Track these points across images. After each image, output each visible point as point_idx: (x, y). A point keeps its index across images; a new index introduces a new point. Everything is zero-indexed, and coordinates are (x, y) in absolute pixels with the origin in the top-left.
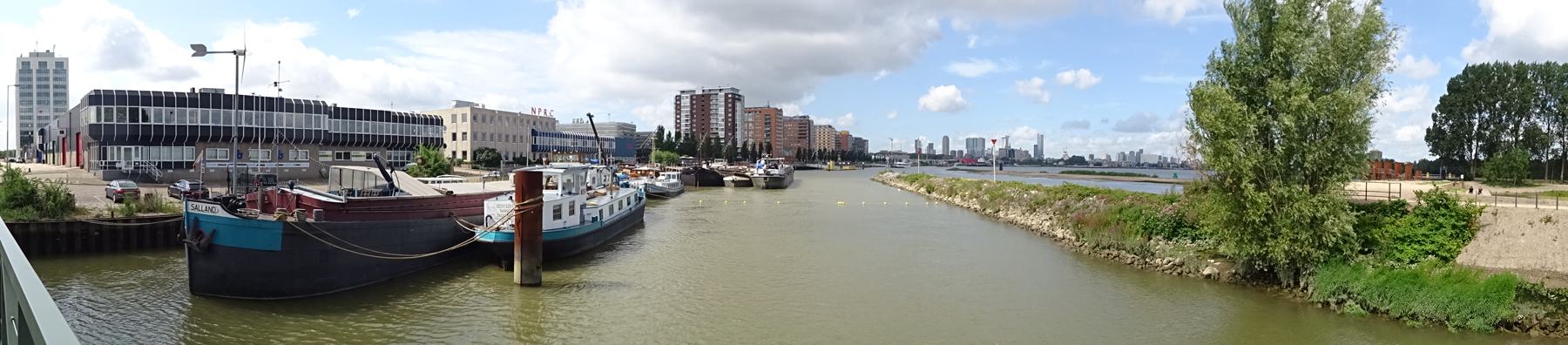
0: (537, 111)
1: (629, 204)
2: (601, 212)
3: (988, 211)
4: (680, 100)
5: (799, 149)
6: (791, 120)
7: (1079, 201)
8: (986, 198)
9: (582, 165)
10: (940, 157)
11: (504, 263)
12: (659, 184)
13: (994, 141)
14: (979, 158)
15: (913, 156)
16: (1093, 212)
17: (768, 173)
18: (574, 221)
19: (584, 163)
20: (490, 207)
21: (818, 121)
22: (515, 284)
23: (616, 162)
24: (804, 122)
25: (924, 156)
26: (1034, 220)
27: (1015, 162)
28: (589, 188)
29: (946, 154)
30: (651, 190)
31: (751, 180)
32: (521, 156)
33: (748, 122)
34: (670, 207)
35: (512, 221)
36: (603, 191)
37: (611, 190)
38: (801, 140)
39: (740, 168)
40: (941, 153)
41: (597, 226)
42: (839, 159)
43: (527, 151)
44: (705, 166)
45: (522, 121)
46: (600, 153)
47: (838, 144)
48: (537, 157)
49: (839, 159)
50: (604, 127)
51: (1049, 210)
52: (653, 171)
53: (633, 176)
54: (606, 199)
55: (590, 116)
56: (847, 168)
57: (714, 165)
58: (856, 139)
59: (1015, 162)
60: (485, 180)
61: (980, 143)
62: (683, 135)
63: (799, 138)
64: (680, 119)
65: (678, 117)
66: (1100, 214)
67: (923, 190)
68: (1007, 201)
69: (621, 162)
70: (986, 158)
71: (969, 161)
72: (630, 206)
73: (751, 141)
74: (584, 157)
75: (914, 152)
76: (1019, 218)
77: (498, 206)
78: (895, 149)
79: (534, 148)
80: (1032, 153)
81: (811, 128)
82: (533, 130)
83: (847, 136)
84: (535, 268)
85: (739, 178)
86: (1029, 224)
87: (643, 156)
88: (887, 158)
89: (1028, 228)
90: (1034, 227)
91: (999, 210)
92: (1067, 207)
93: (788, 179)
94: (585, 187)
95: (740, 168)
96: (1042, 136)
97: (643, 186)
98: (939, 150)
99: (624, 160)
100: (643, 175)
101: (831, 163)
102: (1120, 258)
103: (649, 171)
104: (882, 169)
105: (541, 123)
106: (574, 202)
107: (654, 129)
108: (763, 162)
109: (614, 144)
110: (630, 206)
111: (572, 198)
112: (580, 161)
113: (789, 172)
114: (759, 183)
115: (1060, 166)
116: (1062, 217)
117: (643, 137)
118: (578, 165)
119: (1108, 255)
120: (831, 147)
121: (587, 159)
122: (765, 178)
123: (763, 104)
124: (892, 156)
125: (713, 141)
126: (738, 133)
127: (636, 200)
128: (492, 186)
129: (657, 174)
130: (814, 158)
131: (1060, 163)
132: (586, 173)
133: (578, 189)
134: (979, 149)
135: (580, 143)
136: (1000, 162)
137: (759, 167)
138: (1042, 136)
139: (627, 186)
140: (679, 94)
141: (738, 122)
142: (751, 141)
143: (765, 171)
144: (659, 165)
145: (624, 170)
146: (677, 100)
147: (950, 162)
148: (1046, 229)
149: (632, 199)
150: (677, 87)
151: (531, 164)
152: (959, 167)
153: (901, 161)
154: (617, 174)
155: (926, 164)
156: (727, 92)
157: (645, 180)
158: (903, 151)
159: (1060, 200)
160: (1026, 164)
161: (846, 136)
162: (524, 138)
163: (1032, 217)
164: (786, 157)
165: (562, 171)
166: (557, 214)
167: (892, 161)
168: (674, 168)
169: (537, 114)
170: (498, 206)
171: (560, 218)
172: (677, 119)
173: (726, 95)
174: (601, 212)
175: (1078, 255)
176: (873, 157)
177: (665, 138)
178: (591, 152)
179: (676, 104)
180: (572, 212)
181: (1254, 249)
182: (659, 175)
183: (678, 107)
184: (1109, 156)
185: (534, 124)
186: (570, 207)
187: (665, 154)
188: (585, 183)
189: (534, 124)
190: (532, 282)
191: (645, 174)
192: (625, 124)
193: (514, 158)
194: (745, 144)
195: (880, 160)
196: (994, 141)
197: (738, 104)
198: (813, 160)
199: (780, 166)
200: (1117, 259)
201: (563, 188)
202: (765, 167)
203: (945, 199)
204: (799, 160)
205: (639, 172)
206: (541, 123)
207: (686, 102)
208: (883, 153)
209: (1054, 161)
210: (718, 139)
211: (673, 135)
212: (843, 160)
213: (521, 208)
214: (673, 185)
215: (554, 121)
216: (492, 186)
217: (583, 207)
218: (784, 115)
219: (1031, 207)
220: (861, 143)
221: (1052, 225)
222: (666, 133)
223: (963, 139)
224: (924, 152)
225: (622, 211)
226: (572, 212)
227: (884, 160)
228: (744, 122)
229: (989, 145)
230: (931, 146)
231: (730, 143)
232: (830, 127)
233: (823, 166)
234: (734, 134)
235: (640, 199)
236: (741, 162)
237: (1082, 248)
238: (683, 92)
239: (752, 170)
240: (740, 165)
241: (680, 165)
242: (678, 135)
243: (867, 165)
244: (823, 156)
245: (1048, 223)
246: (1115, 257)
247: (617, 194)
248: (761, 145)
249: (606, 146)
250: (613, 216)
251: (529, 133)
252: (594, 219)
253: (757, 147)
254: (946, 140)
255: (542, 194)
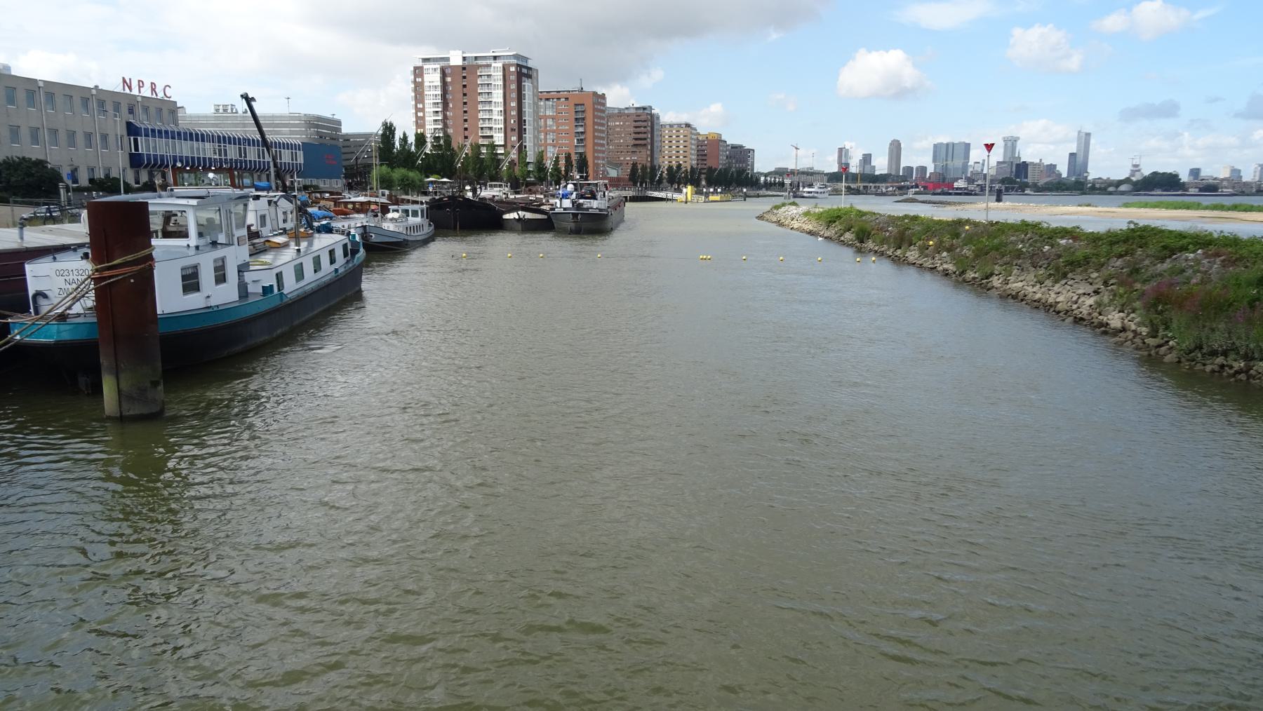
0: (135, 85)
1: (332, 261)
2: (279, 277)
3: (970, 275)
4: (421, 75)
5: (634, 165)
6: (621, 114)
7: (1163, 260)
8: (967, 251)
9: (238, 192)
10: (883, 178)
11: (82, 380)
12: (388, 226)
13: (989, 147)
14: (956, 180)
15: (834, 178)
16: (1194, 281)
17: (579, 206)
18: (226, 295)
19: (242, 187)
20: (38, 276)
21: (667, 116)
22: (109, 418)
23: (305, 188)
24: (643, 118)
25: (854, 177)
26: (1061, 294)
27: (1026, 186)
28: (253, 235)
29: (893, 173)
30: (374, 238)
31: (549, 217)
32: (107, 176)
33: (546, 117)
34: (407, 270)
35: (90, 301)
36: (281, 240)
37: (297, 238)
38: (640, 149)
39: (532, 197)
40: (885, 172)
41: (275, 303)
42: (704, 183)
43: (118, 164)
44: (469, 195)
45: (102, 103)
46: (272, 169)
47: (701, 155)
48: (144, 177)
49: (704, 183)
50: (280, 122)
51: (1095, 275)
52: (376, 203)
53: (338, 213)
54: (288, 255)
55: (248, 100)
56: (717, 198)
57: (486, 193)
58: (734, 147)
59: (1026, 186)
60: (23, 223)
61: (959, 152)
62: (429, 140)
63: (635, 145)
64: (423, 110)
65: (420, 106)
66: (1209, 287)
67: (848, 236)
68: (1007, 259)
69: (316, 187)
70: (970, 180)
71: (937, 185)
72: (336, 266)
73: (551, 153)
74: (241, 177)
75: (836, 170)
76: (1030, 289)
77: (60, 273)
78: (803, 164)
79: (136, 161)
80: (1063, 170)
81: (656, 127)
82: (129, 125)
83: (717, 142)
84: (148, 385)
85: (529, 215)
86: (1051, 300)
87: (357, 177)
88: (787, 181)
89: (1049, 308)
90: (1060, 307)
91: (992, 274)
92: (1135, 271)
93: (615, 215)
94: (244, 232)
95: (532, 197)
96: (1088, 135)
97: (361, 231)
98: (881, 165)
99: (322, 185)
100: (358, 211)
101: (688, 190)
102: (1249, 377)
103: (369, 203)
104: (779, 201)
105: (146, 109)
106: (223, 259)
107: (375, 128)
108: (570, 187)
109: (300, 154)
110: (336, 266)
111: (219, 253)
112: (233, 185)
113: (618, 205)
114: (565, 224)
115: (1123, 193)
116: (1121, 291)
117: (353, 143)
118: (230, 191)
119: (1222, 366)
120: (689, 161)
121: (247, 181)
122: (575, 215)
123: (572, 86)
124: (796, 179)
125: (484, 150)
126: (528, 136)
127: (345, 255)
128: (36, 237)
129: (385, 209)
130: (660, 181)
131: (1123, 188)
132: (246, 205)
133: (230, 235)
134: (958, 163)
135: (232, 153)
136: (997, 186)
137: (565, 196)
138: (1088, 135)
139: (328, 230)
140: (420, 64)
141: (528, 117)
142: (551, 153)
143: (573, 203)
144: (387, 192)
145: (322, 203)
146: (416, 75)
147: (900, 188)
148: (1085, 311)
149: (339, 253)
150: (415, 55)
151: (128, 189)
152: (917, 197)
153: (811, 186)
154: (310, 210)
155: (857, 192)
156: (507, 61)
157: (360, 220)
158: (817, 168)
159: (1120, 256)
160: (1050, 189)
161: (716, 142)
162: (111, 139)
163: (1057, 287)
164: (611, 180)
165: (194, 202)
166: (191, 282)
167: (795, 187)
168: (415, 198)
169: (135, 92)
170: (60, 273)
171: (198, 290)
172: (417, 110)
173: (505, 68)
174: (279, 277)
175: (1151, 361)
176: (762, 179)
177: (397, 144)
178: (256, 169)
179: (415, 82)
180: (221, 278)
181: (397, 183)
182: (388, 211)
183: (419, 89)
184: (1236, 172)
185: (131, 111)
186: (216, 269)
187: (398, 173)
188: (242, 222)
189: (131, 111)
190: (145, 410)
191: (362, 208)
192: (319, 118)
193: (91, 181)
194: (540, 158)
195: (775, 184)
196: (989, 147)
197: (527, 84)
198: (658, 185)
199: (599, 195)
200: (1243, 377)
201: (200, 235)
202: (574, 196)
203: (890, 253)
204: (635, 185)
205: (350, 206)
206: (146, 109)
207: (432, 78)
208: (781, 172)
209: (1110, 183)
210: (493, 147)
211: (411, 139)
212: (709, 184)
213: (107, 273)
214: (417, 228)
215: (171, 109)
216: (36, 237)
217: (243, 268)
218: (608, 105)
219: (1057, 269)
220: (741, 154)
221: (1099, 304)
222: (398, 135)
223: (928, 144)
224: (854, 169)
225: (320, 274)
226: (221, 278)
227: (782, 184)
228: (537, 117)
229: (977, 155)
230: (867, 159)
231: (514, 155)
232: (688, 125)
233: (676, 196)
234: (520, 138)
235: (355, 252)
236: (534, 189)
237: (1163, 349)
238: (426, 60)
239: (552, 201)
240: (531, 192)
241: (425, 194)
242: (421, 139)
243: (752, 193)
244: (676, 178)
245: (1091, 301)
246: (1237, 372)
247: (310, 244)
248: (568, 158)
249: (286, 157)
250: (302, 284)
251: (121, 130)
252: (267, 290)
253: (562, 162)
254: (896, 149)
255: (150, 245)
